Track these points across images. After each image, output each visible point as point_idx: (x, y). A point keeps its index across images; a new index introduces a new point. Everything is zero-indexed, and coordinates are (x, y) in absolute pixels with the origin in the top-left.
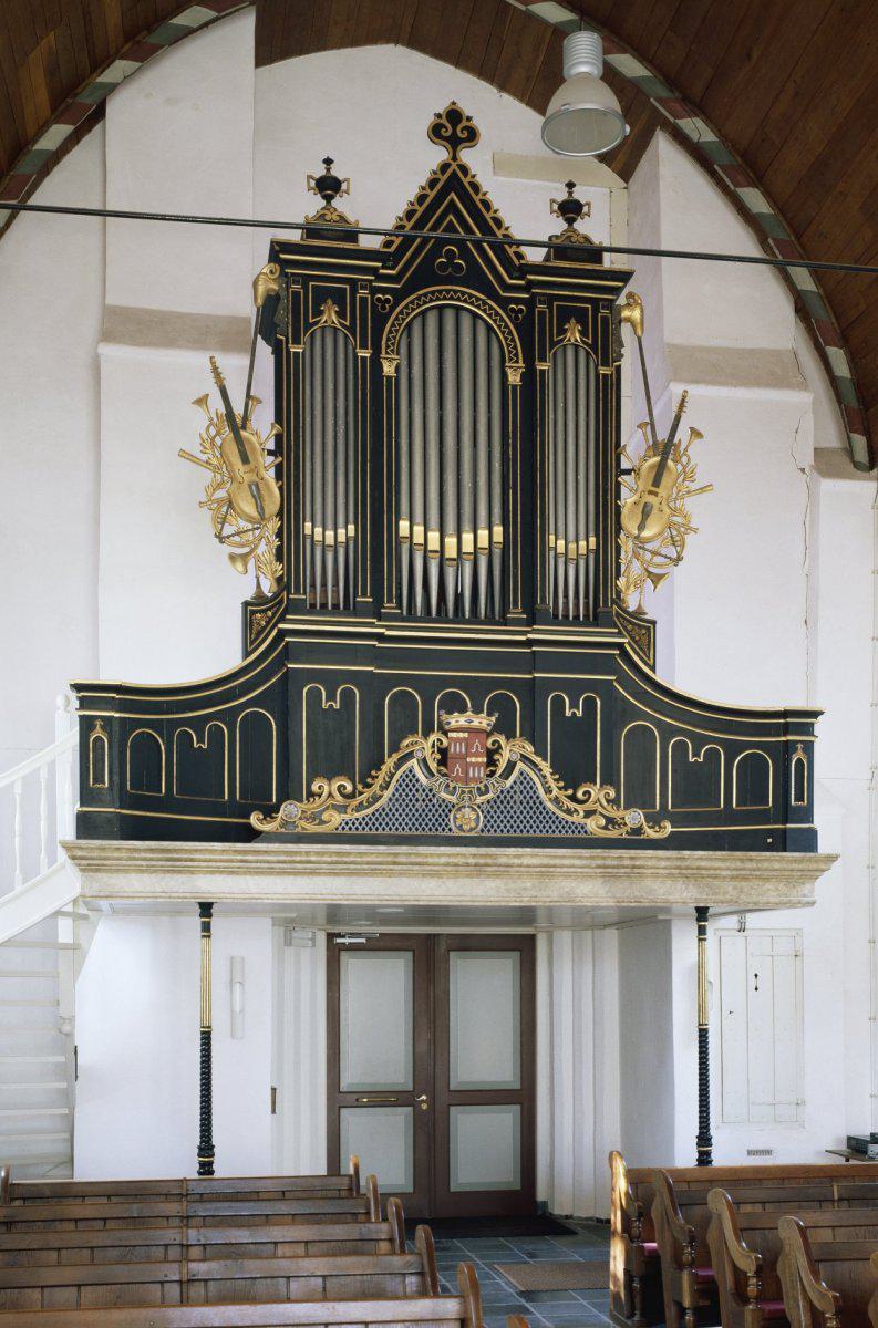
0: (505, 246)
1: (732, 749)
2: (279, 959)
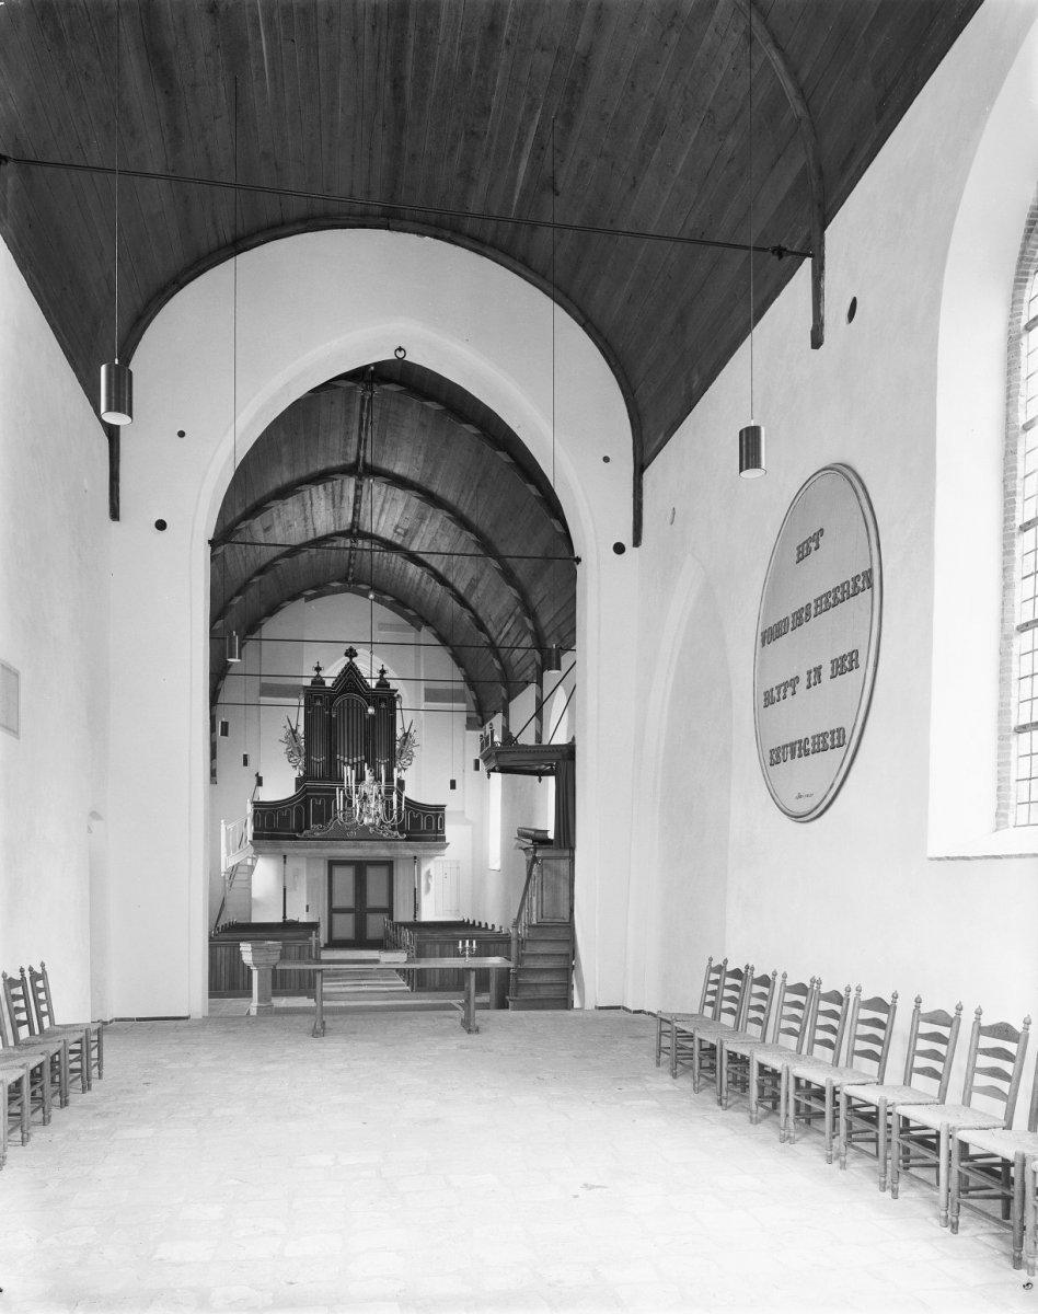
0: (367, 687)
1: (425, 814)
2: (308, 868)
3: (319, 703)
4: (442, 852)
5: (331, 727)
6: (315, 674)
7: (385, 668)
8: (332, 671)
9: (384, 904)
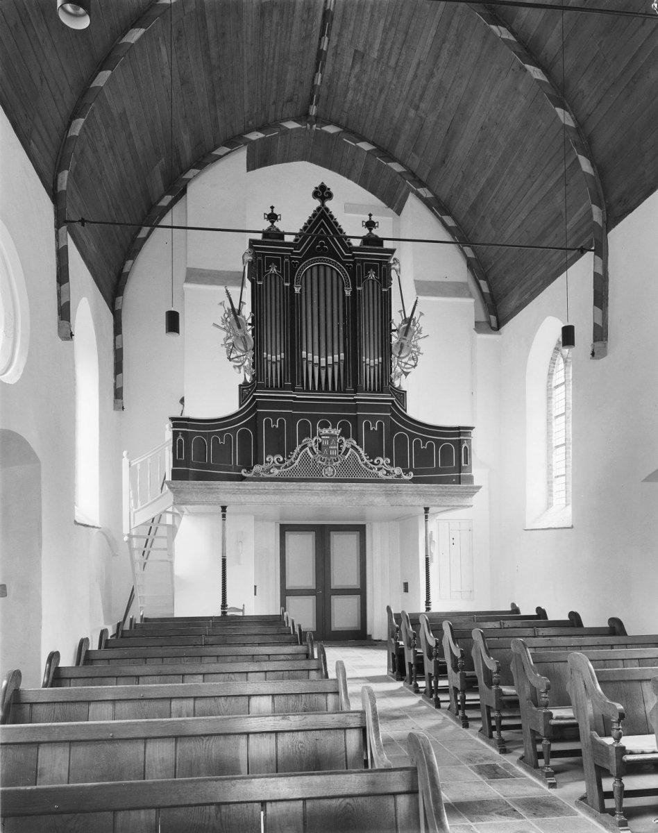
3: (273, 270)
4: (468, 501)
5: (292, 305)
6: (266, 225)
7: (374, 218)
8: (293, 223)
9: (354, 582)
